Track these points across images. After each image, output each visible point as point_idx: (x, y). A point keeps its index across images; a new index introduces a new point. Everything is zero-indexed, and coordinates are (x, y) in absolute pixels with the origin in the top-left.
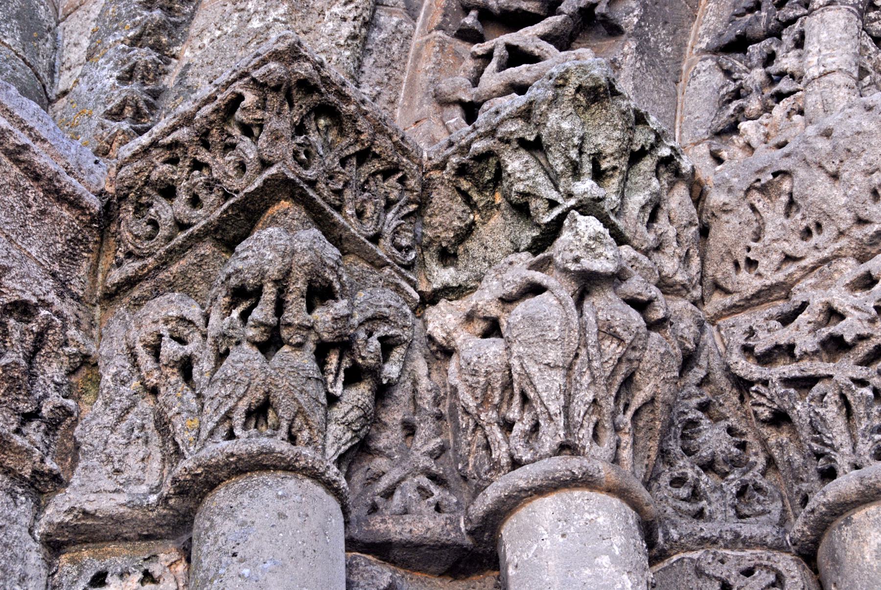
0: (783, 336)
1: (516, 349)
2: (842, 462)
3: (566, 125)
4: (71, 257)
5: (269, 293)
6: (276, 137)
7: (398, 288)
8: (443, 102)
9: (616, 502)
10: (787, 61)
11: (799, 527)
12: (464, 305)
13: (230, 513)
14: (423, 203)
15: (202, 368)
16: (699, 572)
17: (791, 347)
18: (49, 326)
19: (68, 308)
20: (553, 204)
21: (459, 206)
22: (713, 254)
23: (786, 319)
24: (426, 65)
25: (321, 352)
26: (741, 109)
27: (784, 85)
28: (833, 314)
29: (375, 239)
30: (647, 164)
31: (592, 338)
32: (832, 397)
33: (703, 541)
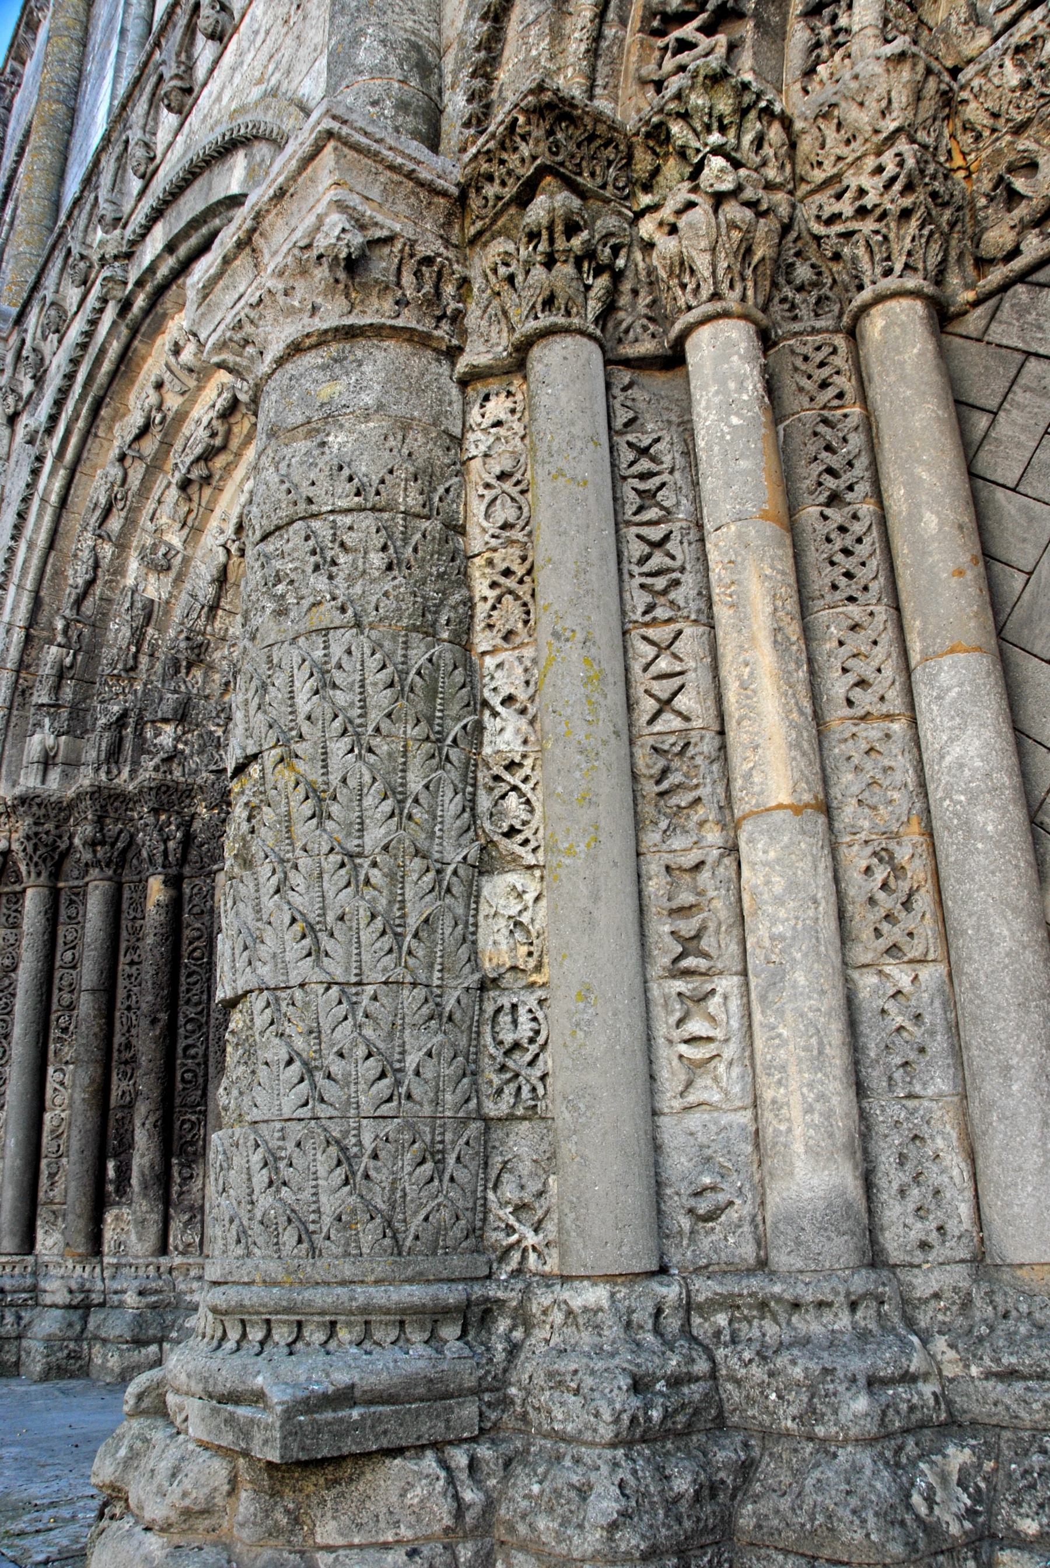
0: (836, 207)
1: (685, 242)
2: (867, 281)
3: (700, 102)
4: (448, 224)
5: (544, 232)
6: (537, 141)
7: (620, 214)
8: (643, 82)
9: (742, 323)
10: (843, 21)
11: (846, 320)
12: (658, 216)
13: (540, 360)
14: (630, 157)
15: (519, 278)
16: (793, 352)
17: (840, 214)
18: (443, 266)
19: (451, 254)
20: (698, 151)
21: (649, 157)
22: (799, 160)
23: (839, 196)
24: (634, 58)
25: (578, 263)
26: (818, 56)
27: (841, 38)
28: (862, 192)
29: (604, 186)
30: (753, 114)
31: (724, 231)
32: (862, 242)
33: (796, 334)
